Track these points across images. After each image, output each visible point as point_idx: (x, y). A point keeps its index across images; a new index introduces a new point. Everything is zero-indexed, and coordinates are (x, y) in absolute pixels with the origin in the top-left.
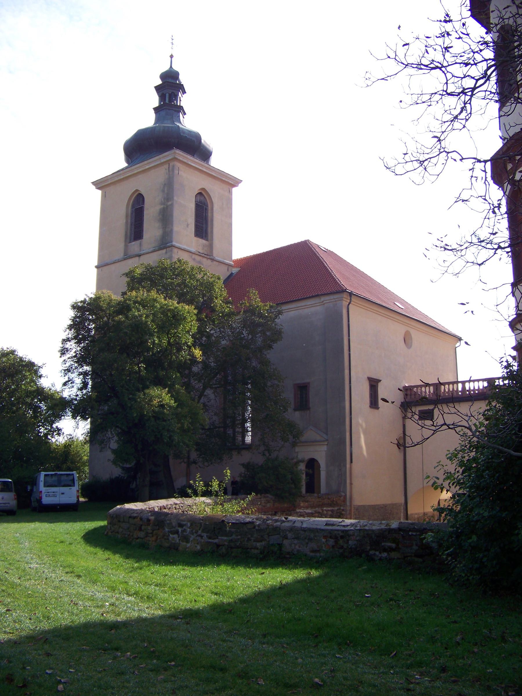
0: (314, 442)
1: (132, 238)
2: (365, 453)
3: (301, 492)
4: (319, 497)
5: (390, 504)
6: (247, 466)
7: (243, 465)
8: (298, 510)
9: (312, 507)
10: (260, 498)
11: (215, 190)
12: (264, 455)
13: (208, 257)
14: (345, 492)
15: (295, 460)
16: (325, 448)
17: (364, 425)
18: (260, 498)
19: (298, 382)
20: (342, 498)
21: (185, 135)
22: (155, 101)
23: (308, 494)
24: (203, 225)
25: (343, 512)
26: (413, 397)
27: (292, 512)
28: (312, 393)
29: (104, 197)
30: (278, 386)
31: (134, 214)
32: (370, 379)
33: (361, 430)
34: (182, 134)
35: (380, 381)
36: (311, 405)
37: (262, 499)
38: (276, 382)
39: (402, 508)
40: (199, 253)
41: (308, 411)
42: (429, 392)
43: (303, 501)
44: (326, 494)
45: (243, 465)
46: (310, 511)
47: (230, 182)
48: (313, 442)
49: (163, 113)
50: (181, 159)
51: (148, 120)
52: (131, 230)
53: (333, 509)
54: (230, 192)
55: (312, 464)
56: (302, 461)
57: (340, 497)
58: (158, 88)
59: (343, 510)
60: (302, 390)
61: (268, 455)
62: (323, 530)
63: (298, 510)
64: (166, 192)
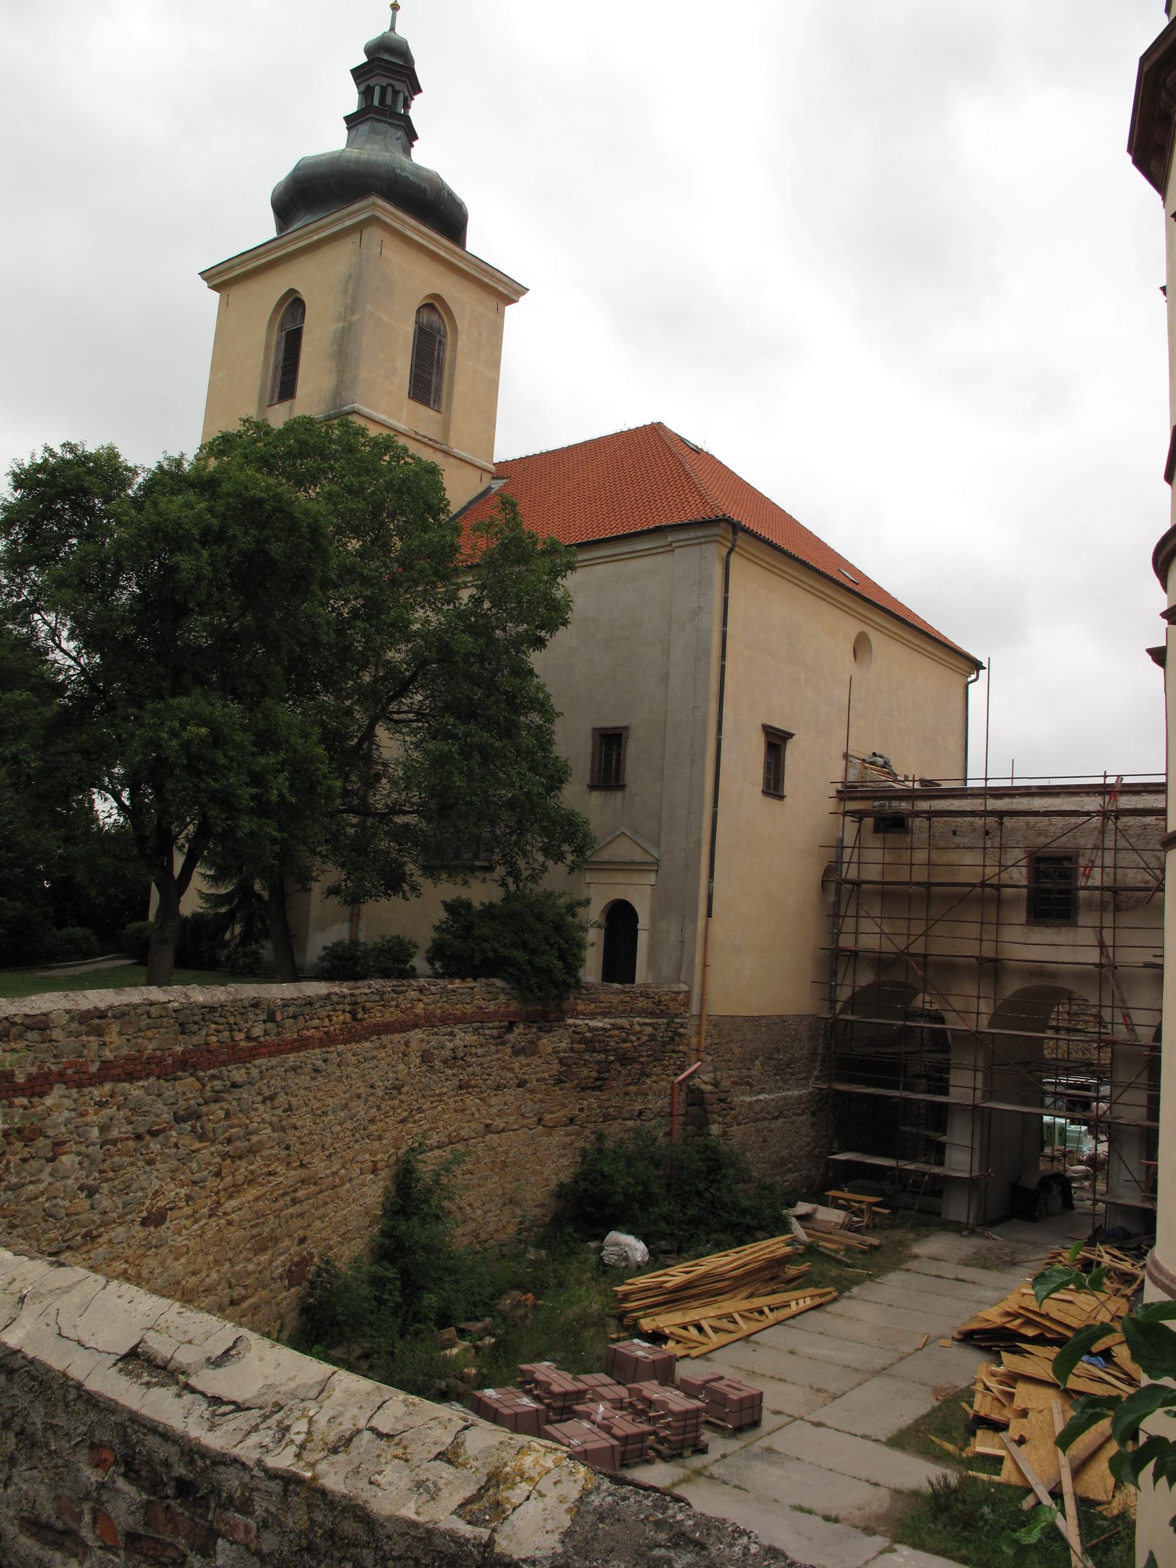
1: (277, 395)
6: (456, 908)
8: (570, 1021)
13: (437, 446)
21: (404, 174)
22: (351, 100)
24: (427, 378)
25: (681, 1030)
28: (632, 749)
29: (224, 306)
31: (283, 343)
32: (768, 731)
34: (398, 171)
35: (792, 735)
40: (416, 433)
46: (600, 1025)
47: (502, 291)
49: (364, 128)
50: (388, 220)
52: (274, 377)
54: (501, 315)
58: (359, 74)
60: (610, 743)
62: (91, 1400)
63: (570, 1021)
64: (350, 292)
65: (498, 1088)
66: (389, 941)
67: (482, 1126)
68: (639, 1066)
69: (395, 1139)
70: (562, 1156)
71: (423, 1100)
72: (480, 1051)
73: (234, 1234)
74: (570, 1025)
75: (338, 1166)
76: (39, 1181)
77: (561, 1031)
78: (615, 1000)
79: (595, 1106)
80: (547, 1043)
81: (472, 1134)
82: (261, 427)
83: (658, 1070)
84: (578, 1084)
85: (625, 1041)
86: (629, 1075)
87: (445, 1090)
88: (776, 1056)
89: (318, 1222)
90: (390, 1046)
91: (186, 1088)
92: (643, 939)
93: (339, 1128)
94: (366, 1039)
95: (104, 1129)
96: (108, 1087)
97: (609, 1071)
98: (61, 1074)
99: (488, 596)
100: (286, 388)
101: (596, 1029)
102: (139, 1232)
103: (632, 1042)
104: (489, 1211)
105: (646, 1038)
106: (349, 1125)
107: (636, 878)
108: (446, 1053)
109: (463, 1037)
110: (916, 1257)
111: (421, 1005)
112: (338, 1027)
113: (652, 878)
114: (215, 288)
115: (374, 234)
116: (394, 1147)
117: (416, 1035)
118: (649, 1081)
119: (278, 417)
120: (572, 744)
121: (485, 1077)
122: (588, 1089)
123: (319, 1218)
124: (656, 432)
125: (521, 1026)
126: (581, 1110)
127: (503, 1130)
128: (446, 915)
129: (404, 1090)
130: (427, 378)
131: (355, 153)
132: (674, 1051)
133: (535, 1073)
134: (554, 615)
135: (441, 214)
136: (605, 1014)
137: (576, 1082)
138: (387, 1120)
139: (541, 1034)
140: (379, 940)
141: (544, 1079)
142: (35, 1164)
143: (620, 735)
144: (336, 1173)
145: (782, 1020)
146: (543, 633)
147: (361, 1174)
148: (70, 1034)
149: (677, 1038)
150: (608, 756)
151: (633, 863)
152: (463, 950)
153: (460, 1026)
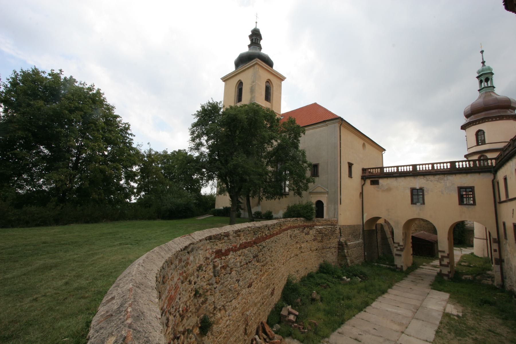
11: (274, 80)
22: (249, 42)
24: (268, 97)
28: (320, 169)
29: (226, 85)
47: (281, 78)
49: (252, 47)
51: (245, 49)
54: (281, 83)
65: (303, 242)
73: (263, 285)
76: (228, 280)
78: (324, 222)
80: (311, 232)
82: (236, 107)
91: (254, 249)
92: (325, 208)
95: (241, 263)
96: (241, 251)
98: (232, 248)
99: (283, 140)
100: (239, 98)
102: (247, 290)
107: (322, 195)
109: (297, 231)
113: (327, 195)
114: (224, 81)
115: (256, 66)
117: (289, 231)
119: (239, 105)
124: (315, 105)
130: (268, 97)
131: (251, 51)
135: (268, 62)
136: (322, 225)
142: (227, 275)
145: (354, 226)
148: (234, 237)
150: (314, 170)
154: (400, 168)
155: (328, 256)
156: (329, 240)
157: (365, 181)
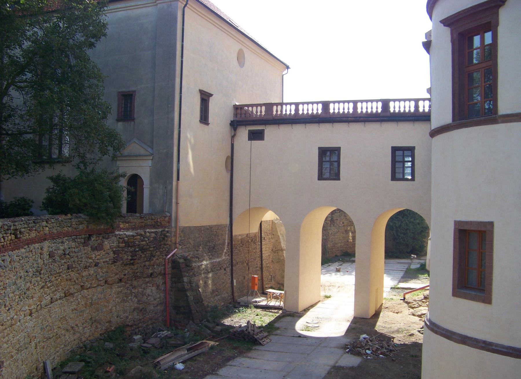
0: (137, 157)
2: (192, 170)
3: (120, 212)
4: (141, 218)
5: (216, 226)
6: (56, 180)
7: (51, 178)
8: (117, 233)
9: (134, 228)
10: (70, 219)
12: (79, 167)
14: (170, 212)
15: (115, 175)
16: (150, 163)
17: (192, 140)
18: (70, 219)
19: (124, 90)
20: (167, 219)
23: (129, 214)
25: (168, 234)
26: (243, 116)
27: (111, 234)
30: (97, 86)
33: (189, 145)
35: (212, 95)
36: (136, 116)
37: (73, 220)
38: (96, 82)
39: (227, 229)
41: (133, 123)
42: (261, 112)
43: (122, 222)
44: (150, 214)
45: (51, 178)
46: (131, 234)
48: (136, 156)
53: (157, 230)
55: (135, 180)
56: (123, 176)
57: (165, 217)
59: (168, 232)
60: (127, 98)
61: (83, 168)
63: (117, 233)
65: (86, 267)
66: (18, 200)
67: (79, 286)
68: (150, 252)
69: (40, 297)
70: (117, 297)
71: (51, 277)
72: (76, 250)
74: (117, 235)
75: (13, 314)
77: (113, 238)
79: (131, 272)
80: (107, 244)
81: (75, 291)
83: (158, 253)
84: (123, 263)
85: (143, 241)
86: (145, 257)
87: (61, 270)
88: (208, 244)
89: (5, 345)
90: (34, 250)
93: (12, 295)
94: (22, 248)
97: (136, 256)
101: (129, 236)
103: (146, 241)
104: (86, 327)
105: (152, 239)
106: (17, 293)
108: (60, 252)
110: (278, 329)
111: (47, 229)
112: (8, 242)
116: (39, 301)
117: (46, 244)
118: (154, 259)
120: (110, 97)
121: (80, 262)
122: (127, 264)
123: (5, 343)
125: (95, 236)
126: (125, 275)
127: (89, 288)
128: (52, 184)
129: (42, 272)
132: (165, 244)
133: (103, 259)
134: (98, 32)
137: (121, 262)
138: (35, 288)
139: (104, 240)
140: (13, 200)
141: (107, 261)
143: (132, 95)
144: (13, 318)
146: (93, 40)
147: (25, 316)
149: (166, 238)
151: (140, 156)
152: (58, 204)
153: (66, 238)
154: (359, 105)
155: (148, 291)
156: (150, 260)
157: (235, 129)
